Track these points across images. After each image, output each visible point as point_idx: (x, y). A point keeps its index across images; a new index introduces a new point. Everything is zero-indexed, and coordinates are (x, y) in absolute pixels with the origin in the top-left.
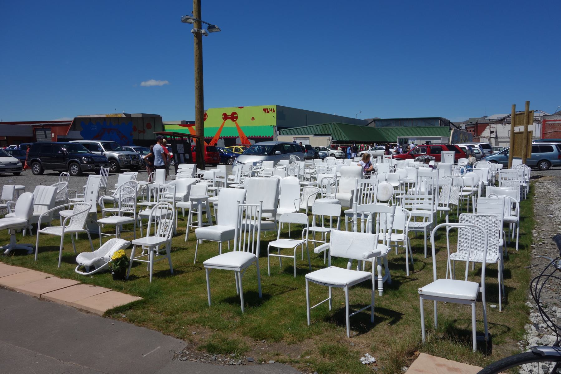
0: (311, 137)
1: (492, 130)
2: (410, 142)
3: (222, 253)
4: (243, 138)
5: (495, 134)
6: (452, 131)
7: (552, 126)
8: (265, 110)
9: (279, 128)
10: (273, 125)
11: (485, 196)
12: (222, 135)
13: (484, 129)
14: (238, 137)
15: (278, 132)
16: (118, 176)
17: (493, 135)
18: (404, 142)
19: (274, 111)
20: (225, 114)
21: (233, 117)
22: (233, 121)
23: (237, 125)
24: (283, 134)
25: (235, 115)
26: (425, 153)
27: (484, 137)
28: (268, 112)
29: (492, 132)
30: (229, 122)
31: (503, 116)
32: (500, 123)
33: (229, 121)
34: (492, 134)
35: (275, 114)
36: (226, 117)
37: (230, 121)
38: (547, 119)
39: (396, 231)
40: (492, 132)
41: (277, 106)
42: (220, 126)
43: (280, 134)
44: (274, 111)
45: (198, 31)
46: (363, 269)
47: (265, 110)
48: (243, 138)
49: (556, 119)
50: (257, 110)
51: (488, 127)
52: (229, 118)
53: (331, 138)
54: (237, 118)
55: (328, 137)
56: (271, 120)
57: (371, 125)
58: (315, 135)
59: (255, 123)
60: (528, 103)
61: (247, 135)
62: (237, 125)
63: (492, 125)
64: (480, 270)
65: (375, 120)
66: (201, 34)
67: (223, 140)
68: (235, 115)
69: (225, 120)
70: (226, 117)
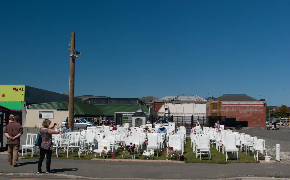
0: (55, 111)
1: (166, 107)
5: (168, 110)
6: (150, 109)
8: (14, 89)
9: (27, 104)
10: (23, 101)
11: (265, 99)
13: (160, 107)
15: (27, 107)
17: (167, 112)
18: (258, 110)
19: (23, 90)
24: (31, 109)
26: (40, 134)
27: (161, 113)
28: (17, 91)
29: (166, 109)
31: (172, 98)
32: (171, 103)
34: (166, 111)
35: (23, 93)
39: (188, 136)
40: (166, 109)
41: (26, 87)
43: (28, 108)
44: (23, 90)
45: (74, 55)
47: (14, 89)
51: (163, 106)
56: (20, 96)
58: (58, 110)
63: (166, 104)
66: (75, 57)
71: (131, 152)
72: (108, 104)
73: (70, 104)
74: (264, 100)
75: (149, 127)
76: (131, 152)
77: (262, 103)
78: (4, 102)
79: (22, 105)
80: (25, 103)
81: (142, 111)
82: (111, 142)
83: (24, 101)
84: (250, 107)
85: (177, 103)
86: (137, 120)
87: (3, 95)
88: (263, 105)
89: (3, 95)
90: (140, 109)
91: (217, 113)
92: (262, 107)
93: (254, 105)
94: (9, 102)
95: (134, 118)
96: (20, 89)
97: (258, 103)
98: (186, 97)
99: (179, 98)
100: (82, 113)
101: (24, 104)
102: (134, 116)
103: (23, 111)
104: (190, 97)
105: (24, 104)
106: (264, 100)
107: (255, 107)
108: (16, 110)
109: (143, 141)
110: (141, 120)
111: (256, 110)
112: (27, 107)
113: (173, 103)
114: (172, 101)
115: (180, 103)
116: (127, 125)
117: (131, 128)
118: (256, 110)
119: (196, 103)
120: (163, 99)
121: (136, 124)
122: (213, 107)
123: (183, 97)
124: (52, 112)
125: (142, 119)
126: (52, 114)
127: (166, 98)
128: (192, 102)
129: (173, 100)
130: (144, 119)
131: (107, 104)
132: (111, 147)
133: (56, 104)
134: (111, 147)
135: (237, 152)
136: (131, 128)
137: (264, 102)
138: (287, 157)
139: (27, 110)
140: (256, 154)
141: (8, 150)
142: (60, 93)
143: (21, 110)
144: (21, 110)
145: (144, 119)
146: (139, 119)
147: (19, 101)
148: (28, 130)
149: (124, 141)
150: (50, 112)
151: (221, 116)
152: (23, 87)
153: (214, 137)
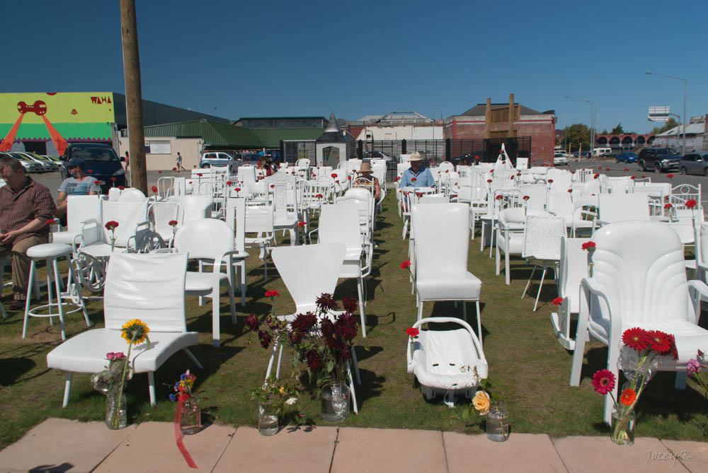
0: (173, 139)
1: (368, 133)
2: (299, 145)
3: (275, 266)
4: (58, 141)
7: (462, 127)
8: (94, 99)
12: (22, 135)
14: (50, 139)
15: (119, 133)
16: (149, 171)
18: (542, 130)
19: (109, 102)
20: (22, 104)
21: (38, 108)
22: (39, 114)
23: (21, 119)
25: (41, 106)
28: (99, 102)
30: (31, 117)
31: (377, 118)
35: (111, 106)
36: (24, 108)
37: (33, 114)
38: (457, 120)
40: (368, 136)
41: (115, 95)
43: (122, 136)
44: (109, 102)
46: (512, 269)
47: (94, 99)
49: (466, 120)
50: (80, 100)
51: (363, 130)
52: (30, 110)
53: (202, 141)
54: (45, 109)
55: (197, 140)
56: (105, 114)
57: (239, 124)
59: (79, 119)
60: (512, 96)
63: (367, 128)
64: (208, 317)
65: (241, 120)
67: (21, 144)
68: (41, 106)
69: (24, 112)
70: (24, 108)
71: (330, 367)
72: (272, 127)
73: (129, 103)
74: (551, 112)
75: (487, 176)
76: (330, 367)
77: (549, 117)
78: (77, 124)
79: (110, 129)
80: (116, 126)
81: (339, 129)
83: (114, 122)
84: (526, 125)
85: (386, 127)
86: (327, 152)
87: (74, 112)
88: (550, 122)
90: (333, 125)
91: (507, 131)
92: (548, 126)
93: (534, 122)
94: (86, 124)
95: (320, 147)
96: (105, 100)
97: (542, 119)
98: (400, 116)
99: (389, 117)
100: (223, 142)
101: (115, 128)
102: (320, 141)
103: (114, 140)
104: (406, 116)
105: (115, 128)
106: (551, 112)
107: (535, 126)
110: (337, 151)
111: (538, 131)
112: (119, 133)
113: (379, 126)
114: (377, 123)
115: (390, 126)
116: (303, 163)
117: (315, 170)
118: (538, 131)
119: (416, 125)
120: (363, 119)
121: (324, 159)
122: (494, 120)
123: (395, 117)
124: (168, 142)
125: (338, 149)
126: (169, 145)
127: (367, 119)
128: (410, 124)
129: (379, 121)
130: (342, 148)
131: (271, 128)
132: (190, 296)
133: (174, 127)
134: (190, 296)
136: (315, 169)
137: (553, 116)
139: (121, 139)
142: (189, 109)
143: (110, 139)
144: (110, 139)
145: (342, 148)
146: (330, 147)
147: (104, 122)
150: (164, 142)
151: (516, 138)
152: (110, 95)
153: (570, 191)
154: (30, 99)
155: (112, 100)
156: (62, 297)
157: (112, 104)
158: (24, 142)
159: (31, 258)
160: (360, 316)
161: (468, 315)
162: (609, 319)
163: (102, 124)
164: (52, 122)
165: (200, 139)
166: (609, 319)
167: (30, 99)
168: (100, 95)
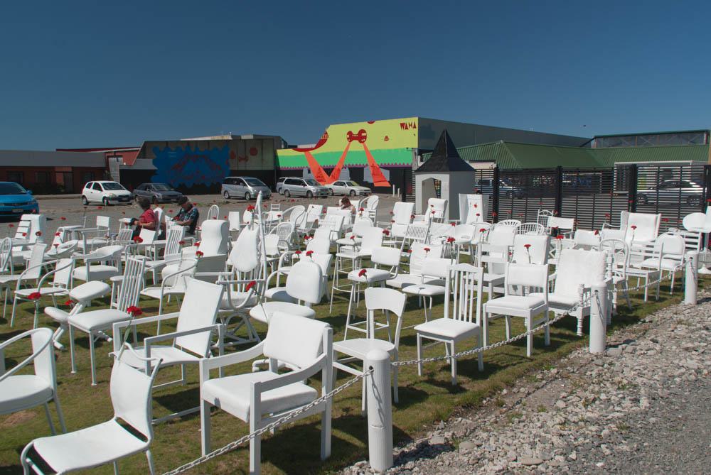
4: (373, 166)
14: (367, 165)
15: (419, 157)
19: (415, 127)
20: (350, 133)
21: (361, 137)
22: (361, 142)
23: (365, 147)
25: (363, 134)
28: (407, 128)
33: (355, 142)
35: (416, 131)
41: (420, 120)
42: (343, 150)
44: (415, 127)
47: (402, 125)
48: (373, 166)
54: (365, 137)
59: (389, 146)
61: (378, 163)
62: (365, 147)
68: (363, 134)
79: (411, 154)
82: (664, 251)
87: (387, 139)
89: (387, 139)
94: (395, 150)
108: (355, 164)
109: (686, 227)
135: (445, 279)
138: (200, 307)
140: (118, 287)
141: (482, 363)
142: (531, 129)
147: (402, 147)
148: (64, 219)
149: (573, 238)
152: (415, 120)
154: (355, 128)
155: (417, 127)
156: (639, 279)
157: (417, 129)
158: (349, 168)
159: (374, 263)
160: (347, 316)
161: (68, 328)
162: (208, 333)
163: (402, 150)
164: (370, 148)
165: (492, 163)
166: (208, 333)
167: (355, 128)
168: (407, 121)
